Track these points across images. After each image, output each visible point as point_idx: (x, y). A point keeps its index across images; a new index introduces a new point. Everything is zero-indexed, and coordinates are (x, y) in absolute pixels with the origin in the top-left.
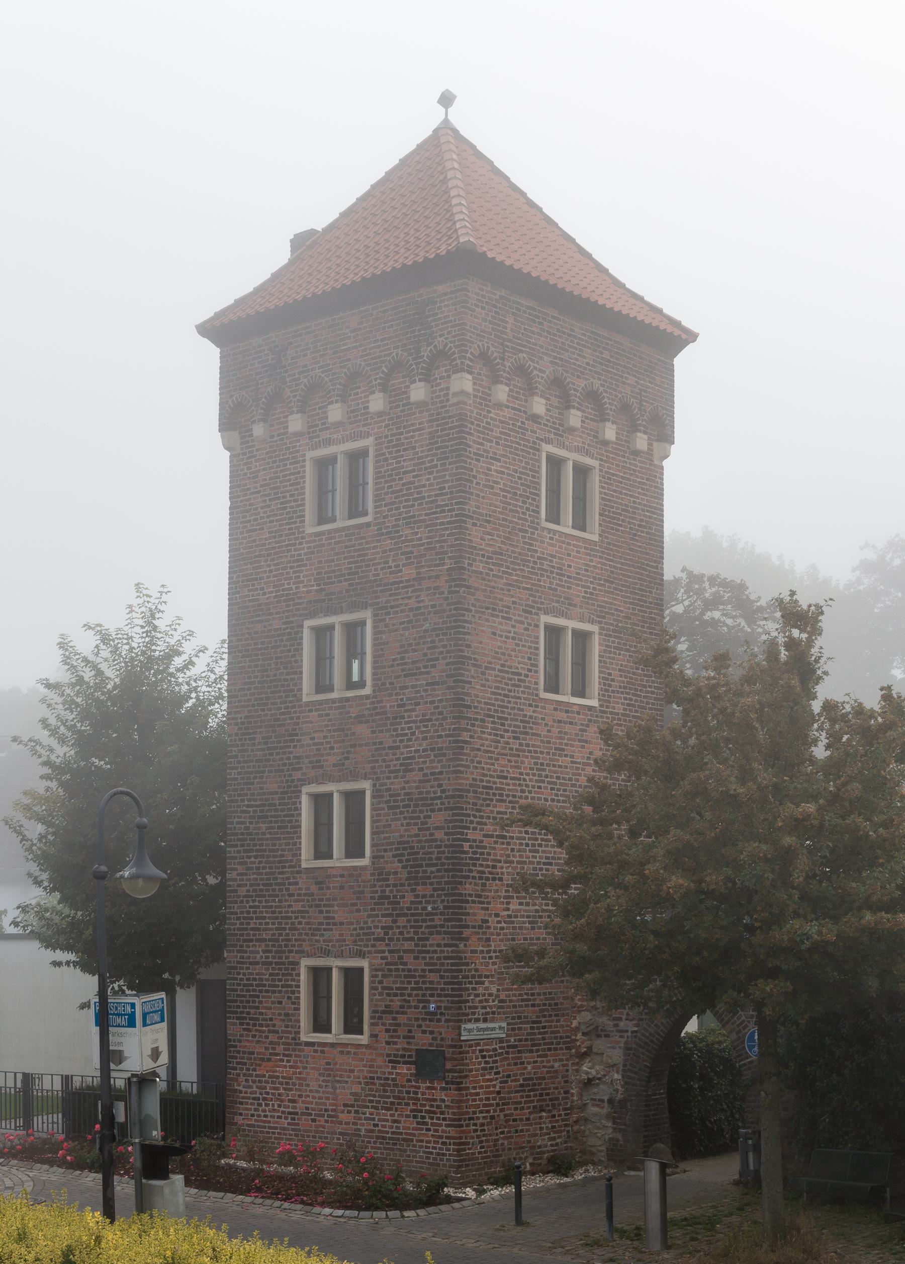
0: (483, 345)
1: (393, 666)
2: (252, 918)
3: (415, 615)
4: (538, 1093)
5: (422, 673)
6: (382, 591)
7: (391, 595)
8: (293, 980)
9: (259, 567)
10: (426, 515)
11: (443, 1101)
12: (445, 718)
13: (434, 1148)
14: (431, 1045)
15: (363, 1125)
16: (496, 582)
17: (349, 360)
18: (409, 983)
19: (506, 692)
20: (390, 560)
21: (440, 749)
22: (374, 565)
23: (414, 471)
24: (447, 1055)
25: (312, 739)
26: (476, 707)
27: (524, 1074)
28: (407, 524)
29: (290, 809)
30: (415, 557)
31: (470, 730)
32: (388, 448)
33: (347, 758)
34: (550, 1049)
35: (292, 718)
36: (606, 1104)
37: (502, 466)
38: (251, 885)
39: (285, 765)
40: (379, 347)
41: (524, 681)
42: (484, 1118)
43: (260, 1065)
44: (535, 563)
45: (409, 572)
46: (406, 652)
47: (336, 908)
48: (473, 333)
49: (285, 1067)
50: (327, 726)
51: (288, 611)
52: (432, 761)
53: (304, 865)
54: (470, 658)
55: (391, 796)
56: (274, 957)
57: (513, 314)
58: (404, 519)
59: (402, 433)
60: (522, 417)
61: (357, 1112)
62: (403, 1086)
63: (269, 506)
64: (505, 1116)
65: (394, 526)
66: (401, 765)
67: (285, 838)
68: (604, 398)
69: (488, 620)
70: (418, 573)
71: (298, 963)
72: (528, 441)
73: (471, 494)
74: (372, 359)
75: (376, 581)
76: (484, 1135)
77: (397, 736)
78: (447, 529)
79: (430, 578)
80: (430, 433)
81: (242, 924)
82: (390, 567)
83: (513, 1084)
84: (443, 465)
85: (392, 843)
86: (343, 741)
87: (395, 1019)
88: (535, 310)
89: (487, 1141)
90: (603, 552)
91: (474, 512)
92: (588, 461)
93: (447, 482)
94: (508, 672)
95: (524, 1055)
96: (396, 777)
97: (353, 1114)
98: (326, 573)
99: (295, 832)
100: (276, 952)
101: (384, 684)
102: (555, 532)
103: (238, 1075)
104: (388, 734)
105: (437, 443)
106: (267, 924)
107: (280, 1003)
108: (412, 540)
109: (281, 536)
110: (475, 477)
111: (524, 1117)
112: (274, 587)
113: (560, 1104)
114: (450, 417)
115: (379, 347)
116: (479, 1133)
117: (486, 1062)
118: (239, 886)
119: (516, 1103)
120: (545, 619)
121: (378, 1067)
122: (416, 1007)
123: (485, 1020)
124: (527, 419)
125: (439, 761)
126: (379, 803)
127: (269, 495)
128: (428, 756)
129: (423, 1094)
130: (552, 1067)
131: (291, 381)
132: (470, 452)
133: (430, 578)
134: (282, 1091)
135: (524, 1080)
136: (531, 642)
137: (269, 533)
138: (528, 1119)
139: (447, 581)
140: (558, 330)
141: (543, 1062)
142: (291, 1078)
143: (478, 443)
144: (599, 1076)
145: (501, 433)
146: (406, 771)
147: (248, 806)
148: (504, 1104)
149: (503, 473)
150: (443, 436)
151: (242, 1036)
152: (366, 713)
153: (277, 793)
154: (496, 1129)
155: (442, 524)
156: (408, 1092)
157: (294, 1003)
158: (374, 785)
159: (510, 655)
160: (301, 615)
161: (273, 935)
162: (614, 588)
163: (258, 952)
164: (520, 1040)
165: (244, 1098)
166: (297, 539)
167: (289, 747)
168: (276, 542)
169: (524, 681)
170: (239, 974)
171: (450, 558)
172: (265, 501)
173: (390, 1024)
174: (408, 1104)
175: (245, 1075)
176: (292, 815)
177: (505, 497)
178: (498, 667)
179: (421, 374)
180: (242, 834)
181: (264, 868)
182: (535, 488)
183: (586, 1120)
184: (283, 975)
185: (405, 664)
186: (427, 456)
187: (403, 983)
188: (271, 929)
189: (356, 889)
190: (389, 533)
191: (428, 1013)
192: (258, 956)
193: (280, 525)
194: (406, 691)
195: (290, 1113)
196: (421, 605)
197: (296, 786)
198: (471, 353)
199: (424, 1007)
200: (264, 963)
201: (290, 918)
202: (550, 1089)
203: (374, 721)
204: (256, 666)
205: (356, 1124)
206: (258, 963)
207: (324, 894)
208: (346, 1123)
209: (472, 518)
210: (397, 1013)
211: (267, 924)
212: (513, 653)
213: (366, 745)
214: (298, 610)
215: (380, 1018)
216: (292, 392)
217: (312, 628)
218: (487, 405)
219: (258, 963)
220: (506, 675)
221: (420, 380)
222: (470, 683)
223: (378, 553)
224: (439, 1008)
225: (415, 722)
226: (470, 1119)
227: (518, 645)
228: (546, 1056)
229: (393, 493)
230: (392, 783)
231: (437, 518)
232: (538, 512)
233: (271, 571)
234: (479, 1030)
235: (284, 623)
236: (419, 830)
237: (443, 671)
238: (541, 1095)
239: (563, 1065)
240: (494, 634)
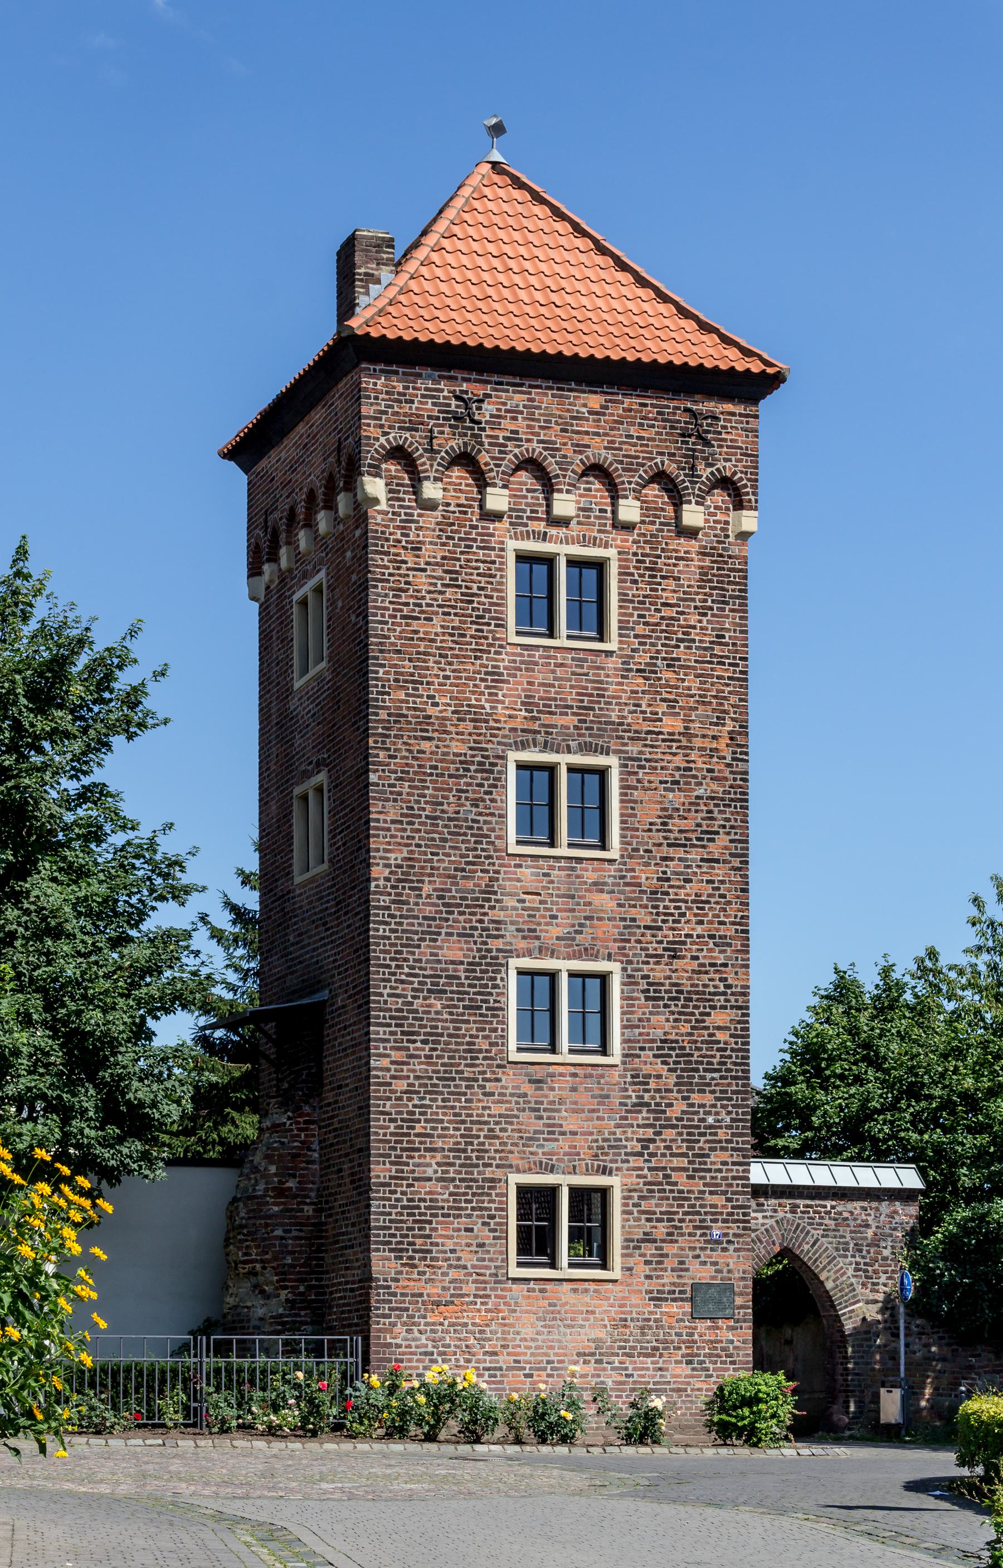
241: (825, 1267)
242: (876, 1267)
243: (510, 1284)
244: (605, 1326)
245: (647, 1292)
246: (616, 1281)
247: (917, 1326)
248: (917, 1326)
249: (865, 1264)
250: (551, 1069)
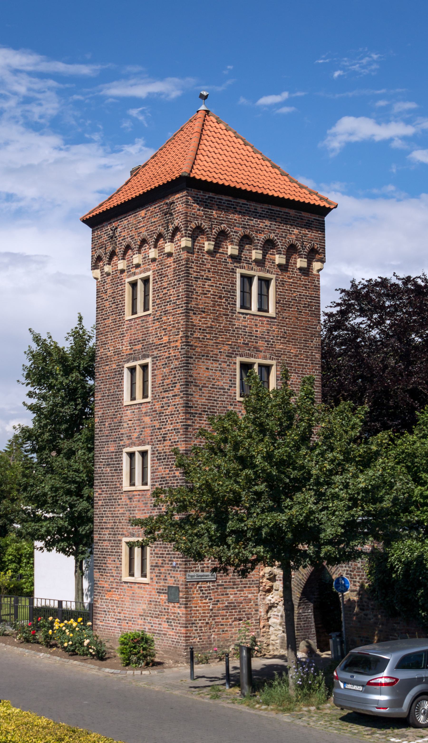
0: (198, 223)
1: (159, 387)
2: (103, 517)
3: (168, 361)
4: (237, 610)
5: (170, 390)
6: (155, 349)
7: (159, 351)
8: (120, 549)
9: (108, 338)
10: (173, 309)
11: (179, 614)
12: (179, 413)
13: (175, 639)
14: (174, 584)
15: (147, 626)
16: (208, 342)
17: (141, 233)
18: (165, 551)
19: (216, 399)
20: (158, 332)
21: (178, 429)
22: (152, 335)
23: (167, 287)
24: (180, 589)
25: (128, 424)
26: (196, 407)
27: (228, 600)
28: (165, 314)
29: (119, 461)
30: (168, 331)
31: (192, 419)
32: (157, 276)
33: (141, 434)
34: (245, 587)
35: (120, 414)
36: (280, 618)
37: (212, 283)
38: (104, 500)
39: (117, 438)
40: (152, 226)
41: (227, 392)
42: (202, 623)
43: (106, 594)
44: (234, 331)
45: (165, 339)
46: (164, 379)
47: (137, 512)
48: (191, 217)
49: (116, 595)
50: (133, 418)
51: (119, 359)
52: (174, 436)
53: (125, 489)
54: (192, 382)
55: (158, 453)
56: (112, 537)
57: (217, 205)
58: (164, 312)
59: (162, 269)
60: (224, 257)
61: (144, 619)
62: (163, 606)
63: (111, 307)
64: (216, 622)
65: (160, 316)
66: (163, 437)
67: (117, 476)
68: (277, 242)
69: (203, 362)
70: (169, 339)
71: (120, 540)
72: (228, 268)
73: (193, 298)
74: (150, 232)
75: (152, 343)
76: (201, 633)
77: (161, 422)
78: (180, 316)
79: (174, 341)
80: (174, 268)
81: (100, 520)
82: (158, 336)
83: (221, 605)
84: (179, 284)
85: (158, 478)
86: (140, 425)
87: (159, 570)
88: (231, 201)
89: (203, 636)
90: (279, 323)
91: (194, 307)
92: (268, 275)
93: (180, 292)
94: (216, 388)
95: (228, 590)
96: (160, 444)
97: (143, 620)
98: (134, 340)
99: (121, 473)
100: (113, 534)
101: (156, 396)
102: (247, 314)
103: (98, 599)
104: (157, 422)
105: (176, 273)
106: (110, 520)
107: (114, 561)
108: (167, 323)
109: (116, 322)
110: (194, 289)
111: (228, 624)
112: (114, 347)
113: (252, 617)
114: (182, 260)
115: (152, 226)
116: (198, 631)
117: (203, 594)
118: (99, 500)
119: (223, 616)
120: (239, 359)
121: (153, 595)
122: (168, 564)
123: (203, 571)
124: (228, 257)
125: (177, 435)
126: (153, 457)
127: (111, 301)
128: (173, 433)
129: (171, 610)
130: (247, 597)
131: (119, 244)
132: (191, 277)
133: (174, 341)
134: (115, 607)
135: (228, 603)
136: (232, 372)
137: (112, 320)
138: (230, 625)
139: (181, 343)
140: (246, 210)
141: (241, 594)
142: (118, 601)
143: (197, 272)
144: (276, 602)
145: (211, 266)
146: (164, 440)
147: (103, 459)
148: (214, 616)
149: (213, 286)
150: (179, 269)
151: (99, 578)
152: (149, 411)
153: (113, 452)
154: (210, 629)
155: (179, 314)
156: (165, 609)
157: (120, 561)
158: (152, 448)
159: (218, 380)
160: (124, 361)
161: (112, 525)
162: (287, 341)
163: (106, 535)
164: (226, 582)
165: (100, 611)
166: (122, 323)
167: (118, 428)
168: (114, 325)
169: (227, 392)
170: (98, 546)
171: (182, 331)
172: (110, 304)
173: (158, 573)
174: (164, 615)
175: (101, 599)
176: (119, 464)
177: (214, 298)
178: (211, 386)
179: (169, 239)
180: (100, 473)
181: (109, 491)
182: (234, 292)
183: (270, 626)
184: (116, 546)
185: (164, 386)
186: (172, 280)
187: (163, 551)
188: (111, 523)
189: (145, 502)
190: (158, 319)
191: (172, 567)
192: (106, 536)
193: (116, 316)
194: (164, 399)
195: (118, 619)
196: (170, 355)
197: (121, 449)
198: (191, 227)
199: (171, 564)
200: (109, 540)
201: (118, 517)
202: (245, 608)
203: (152, 415)
204: (106, 388)
205: (144, 625)
206: (106, 540)
207: (132, 505)
208: (141, 625)
209: (193, 310)
210: (161, 567)
211: (110, 520)
212: (220, 378)
213: (149, 427)
214: (122, 359)
215: (154, 569)
216: (119, 249)
217: (128, 368)
218: (201, 252)
219: (106, 540)
220: (215, 390)
221: (169, 242)
222: (192, 395)
223: (153, 329)
224: (177, 564)
225: (168, 415)
226: (193, 624)
227: (223, 374)
228: (243, 591)
229: (159, 299)
230: (159, 447)
231: (176, 311)
232: (235, 305)
233: (112, 339)
234: (198, 576)
235: (117, 366)
236: (170, 471)
237: (179, 389)
238: (240, 612)
239: (255, 596)
240: (207, 369)
241: (334, 572)
242: (355, 573)
243: (123, 584)
244: (146, 604)
245: (157, 589)
246: (148, 584)
247: (372, 605)
248: (372, 605)
249: (351, 571)
250: (135, 493)
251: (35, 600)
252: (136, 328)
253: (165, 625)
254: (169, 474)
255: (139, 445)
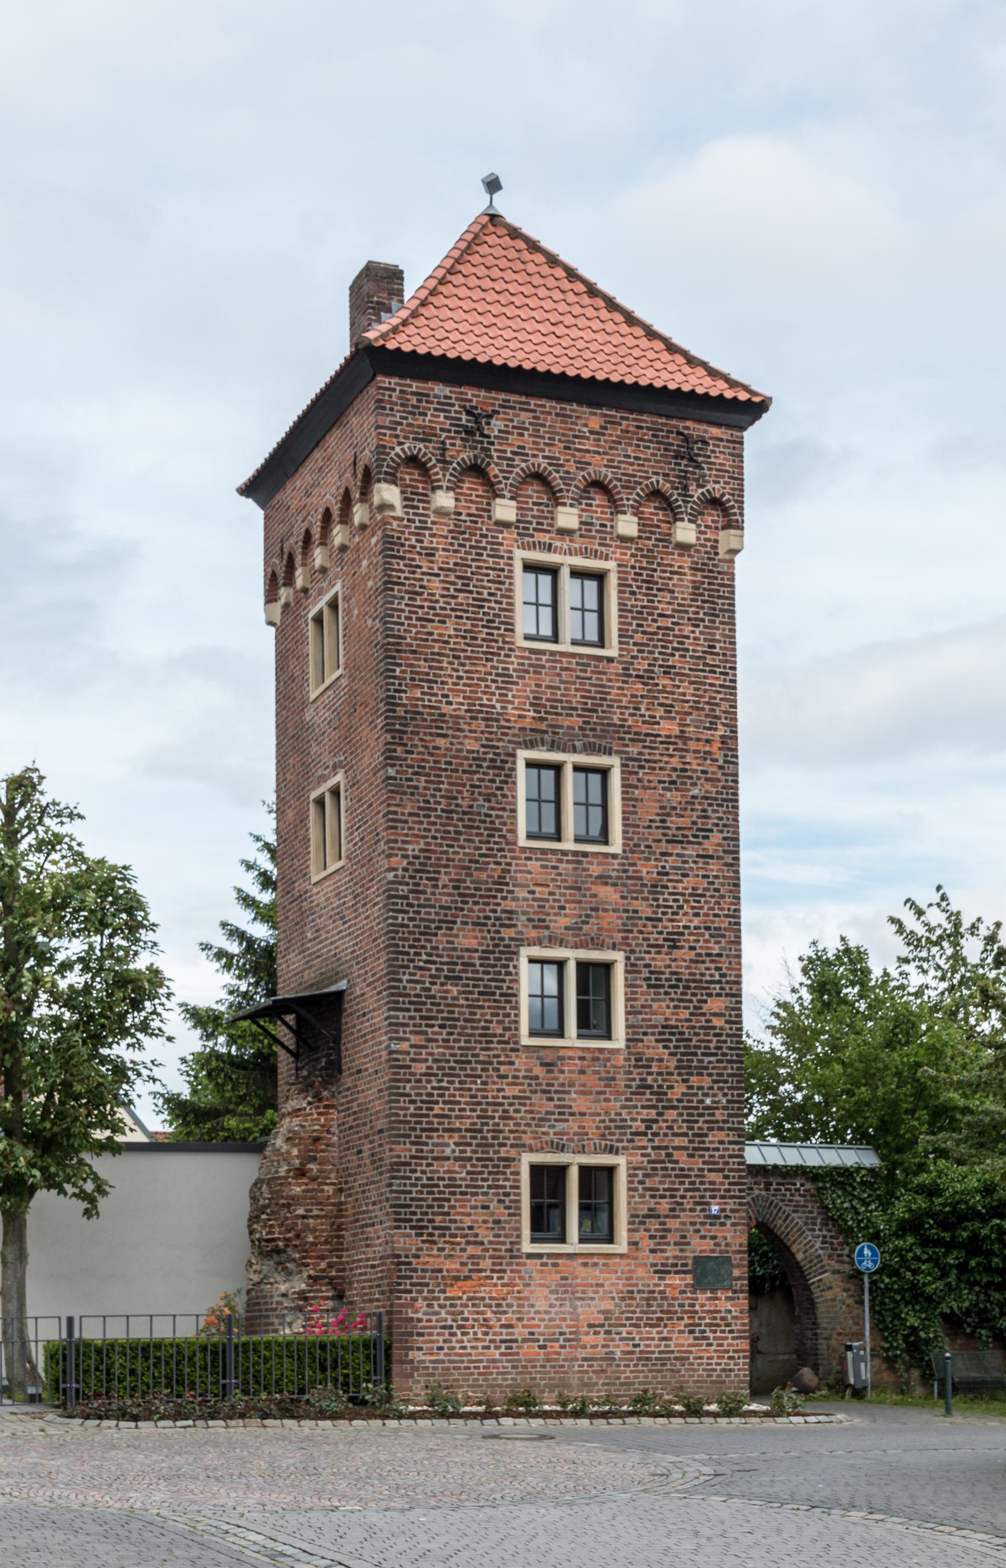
14: (712, 1251)
47: (574, 1096)
61: (607, 1332)
158: (628, 958)
231: (705, 677)
244: (613, 1298)
251: (30, 1324)
252: (559, 675)
253: (688, 1340)
254: (689, 1020)
255: (576, 947)
